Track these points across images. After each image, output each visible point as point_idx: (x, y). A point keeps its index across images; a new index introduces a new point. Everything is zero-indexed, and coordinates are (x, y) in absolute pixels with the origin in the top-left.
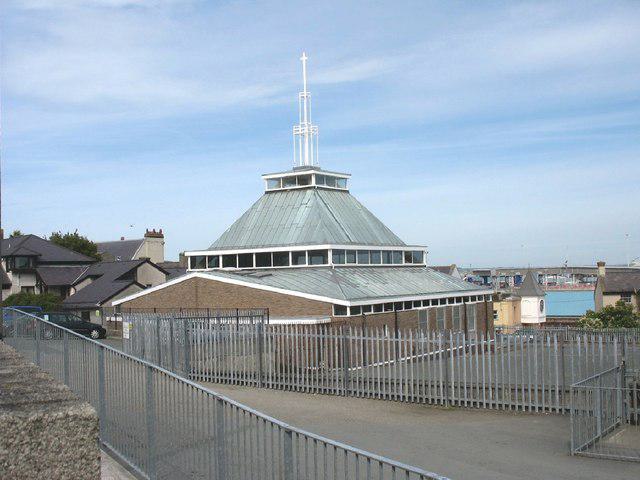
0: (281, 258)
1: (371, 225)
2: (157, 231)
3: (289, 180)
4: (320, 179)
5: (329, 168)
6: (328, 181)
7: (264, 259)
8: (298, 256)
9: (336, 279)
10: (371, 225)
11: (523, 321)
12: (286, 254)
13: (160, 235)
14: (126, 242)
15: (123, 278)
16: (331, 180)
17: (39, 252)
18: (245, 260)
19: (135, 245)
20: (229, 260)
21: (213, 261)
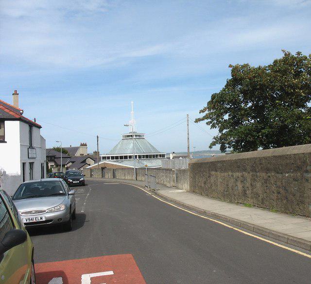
0: (126, 157)
1: (150, 148)
2: (85, 143)
3: (129, 136)
4: (136, 136)
5: (139, 132)
6: (139, 136)
7: (121, 157)
8: (130, 157)
9: (139, 162)
10: (150, 148)
11: (50, 145)
12: (127, 156)
13: (86, 145)
14: (73, 148)
15: (82, 162)
16: (139, 136)
17: (55, 155)
18: (117, 158)
19: (76, 149)
20: (113, 158)
21: (108, 158)
